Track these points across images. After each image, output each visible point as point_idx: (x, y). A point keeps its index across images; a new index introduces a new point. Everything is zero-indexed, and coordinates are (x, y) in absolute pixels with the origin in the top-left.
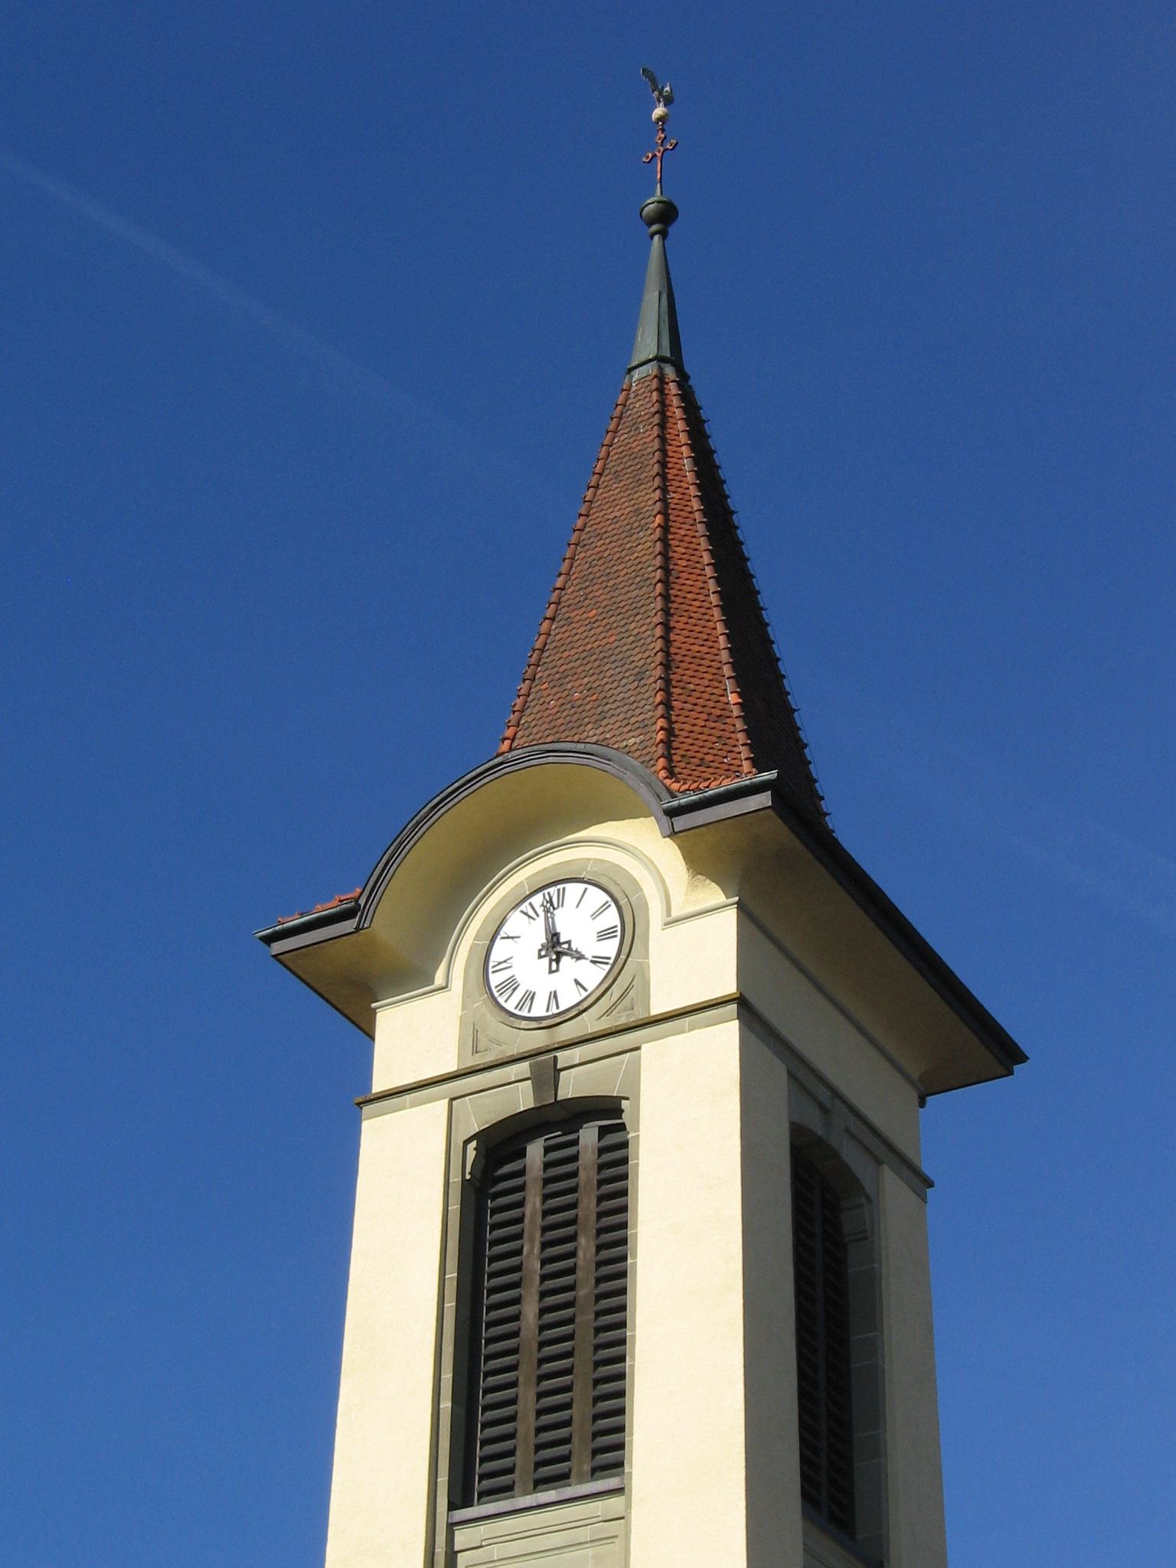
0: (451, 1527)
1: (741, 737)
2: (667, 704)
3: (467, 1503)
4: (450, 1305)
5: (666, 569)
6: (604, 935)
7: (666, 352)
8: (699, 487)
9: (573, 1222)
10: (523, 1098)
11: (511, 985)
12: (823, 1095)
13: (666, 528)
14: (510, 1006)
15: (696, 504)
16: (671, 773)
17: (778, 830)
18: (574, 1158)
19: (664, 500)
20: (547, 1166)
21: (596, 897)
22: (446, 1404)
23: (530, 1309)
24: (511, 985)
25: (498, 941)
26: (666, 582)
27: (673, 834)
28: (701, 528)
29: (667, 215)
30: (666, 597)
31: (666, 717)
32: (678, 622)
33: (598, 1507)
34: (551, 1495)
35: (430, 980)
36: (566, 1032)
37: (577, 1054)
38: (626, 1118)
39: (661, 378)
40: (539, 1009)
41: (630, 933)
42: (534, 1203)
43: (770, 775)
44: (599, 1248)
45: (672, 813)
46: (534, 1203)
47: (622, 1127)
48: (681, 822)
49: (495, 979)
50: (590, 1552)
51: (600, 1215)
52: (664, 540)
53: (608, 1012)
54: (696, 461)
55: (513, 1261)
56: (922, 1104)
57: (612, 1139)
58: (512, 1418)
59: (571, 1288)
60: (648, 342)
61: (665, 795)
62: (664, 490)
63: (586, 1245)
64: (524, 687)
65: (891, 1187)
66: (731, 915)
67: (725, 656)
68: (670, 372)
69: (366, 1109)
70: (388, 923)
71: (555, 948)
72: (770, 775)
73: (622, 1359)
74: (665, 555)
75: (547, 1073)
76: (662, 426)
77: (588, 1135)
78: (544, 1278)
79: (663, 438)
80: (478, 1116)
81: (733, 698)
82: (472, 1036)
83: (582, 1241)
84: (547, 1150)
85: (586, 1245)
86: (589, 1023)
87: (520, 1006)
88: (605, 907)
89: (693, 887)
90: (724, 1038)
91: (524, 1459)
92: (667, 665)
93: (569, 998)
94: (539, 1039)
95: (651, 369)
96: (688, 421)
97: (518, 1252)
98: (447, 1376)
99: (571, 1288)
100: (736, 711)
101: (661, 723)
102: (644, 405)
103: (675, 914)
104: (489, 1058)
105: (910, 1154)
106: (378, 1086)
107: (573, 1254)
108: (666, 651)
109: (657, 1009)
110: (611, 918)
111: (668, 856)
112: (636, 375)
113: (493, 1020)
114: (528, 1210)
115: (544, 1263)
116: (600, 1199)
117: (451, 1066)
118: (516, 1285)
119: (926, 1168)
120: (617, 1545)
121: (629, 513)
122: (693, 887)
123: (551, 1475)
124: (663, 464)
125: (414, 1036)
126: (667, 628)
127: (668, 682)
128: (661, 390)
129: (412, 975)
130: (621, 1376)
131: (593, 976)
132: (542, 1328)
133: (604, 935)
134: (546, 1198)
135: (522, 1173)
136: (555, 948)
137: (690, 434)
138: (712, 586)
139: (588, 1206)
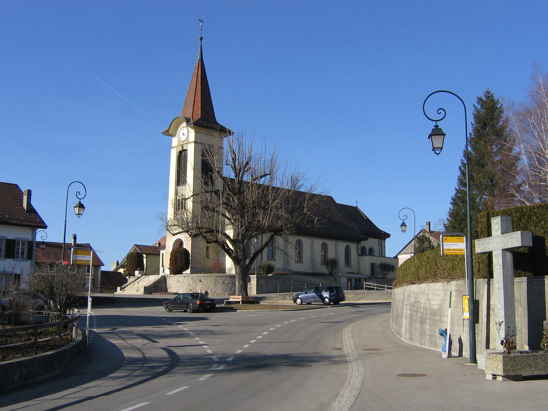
36: (184, 143)
75: (183, 147)
125: (175, 141)
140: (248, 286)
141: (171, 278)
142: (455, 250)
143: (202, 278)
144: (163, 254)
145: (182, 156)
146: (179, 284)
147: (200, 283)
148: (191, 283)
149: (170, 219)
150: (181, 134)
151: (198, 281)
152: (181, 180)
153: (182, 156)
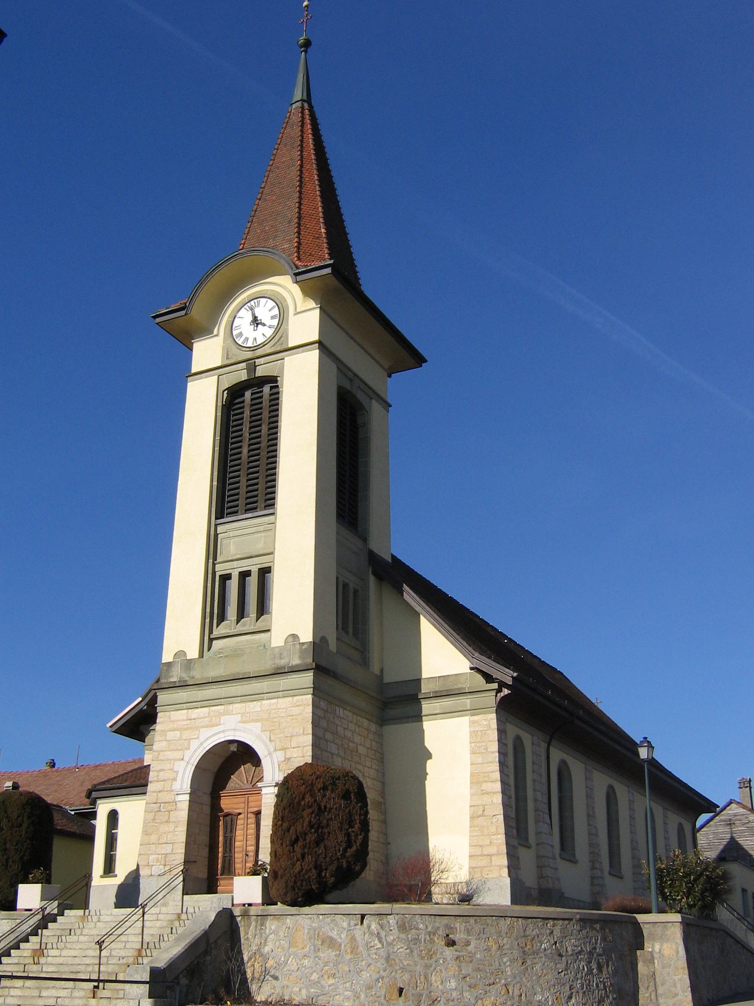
0: (216, 525)
1: (325, 245)
2: (299, 233)
3: (222, 517)
4: (217, 448)
5: (300, 181)
6: (273, 318)
7: (305, 98)
8: (315, 150)
9: (260, 420)
10: (243, 376)
11: (241, 334)
12: (350, 374)
13: (301, 166)
14: (240, 343)
15: (313, 157)
16: (299, 259)
17: (334, 282)
18: (261, 397)
19: (301, 155)
20: (252, 400)
21: (271, 304)
22: (215, 483)
23: (245, 450)
24: (241, 334)
25: (236, 319)
26: (300, 186)
27: (297, 282)
28: (314, 166)
29: (307, 44)
30: (300, 192)
31: (298, 237)
32: (304, 202)
33: (266, 519)
34: (250, 515)
35: (215, 332)
36: (259, 352)
37: (262, 360)
38: (279, 383)
39: (302, 107)
40: (250, 344)
41: (282, 317)
42: (247, 413)
43: (332, 262)
44: (269, 429)
45: (296, 274)
46: (247, 413)
47: (277, 386)
48: (299, 278)
49: (235, 333)
50: (263, 534)
51: (270, 418)
52: (301, 171)
53: (274, 345)
54: (314, 140)
55: (240, 433)
56: (390, 376)
57: (274, 391)
58: (238, 488)
59: (259, 443)
60: (298, 94)
61: (294, 268)
62: (302, 151)
63: (264, 428)
64: (249, 225)
65: (376, 408)
66: (317, 312)
67: (321, 214)
68: (306, 105)
69: (189, 379)
70: (197, 312)
71: (256, 322)
72: (332, 262)
73: (275, 468)
74: (301, 176)
75: (252, 366)
76: (302, 126)
77: (266, 389)
78: (250, 439)
79: (302, 131)
80: (229, 381)
81: (323, 230)
82: (227, 354)
83: (263, 426)
84: (252, 394)
85: (264, 428)
86: (267, 349)
87: (243, 342)
88: (274, 307)
89: (304, 301)
90: (314, 355)
91: (242, 502)
92: (299, 218)
93: (260, 340)
94: (249, 355)
95: (299, 104)
96: (312, 125)
97: (242, 430)
98: (216, 473)
99: (259, 443)
100: (324, 235)
101: (296, 240)
102: (296, 118)
103: (298, 310)
104: (232, 361)
105: (383, 395)
106: (193, 371)
107: (260, 431)
108: (299, 213)
109: (290, 345)
110: (276, 311)
111: (296, 289)
112: (294, 106)
113: (234, 347)
114: (245, 415)
115: (250, 434)
116: (270, 412)
117: (219, 364)
118: (240, 441)
119: (389, 401)
120: (271, 533)
121: (288, 161)
122: (304, 301)
123: (251, 508)
124: (302, 141)
125: (206, 352)
126: (300, 203)
127: (299, 224)
128: (302, 113)
129: (206, 331)
130: (275, 474)
131: (269, 332)
132: (249, 457)
133: (273, 318)
134: (251, 411)
135: (243, 402)
136: (256, 322)
137: (312, 130)
138: (318, 188)
139: (266, 414)
140: (641, 968)
141: (271, 925)
142: (111, 842)
143: (458, 924)
144: (113, 816)
145: (249, 407)
146: (328, 954)
147: (449, 952)
148: (401, 949)
149: (181, 654)
150: (245, 316)
151: (440, 942)
152: (244, 483)
153: (249, 407)
